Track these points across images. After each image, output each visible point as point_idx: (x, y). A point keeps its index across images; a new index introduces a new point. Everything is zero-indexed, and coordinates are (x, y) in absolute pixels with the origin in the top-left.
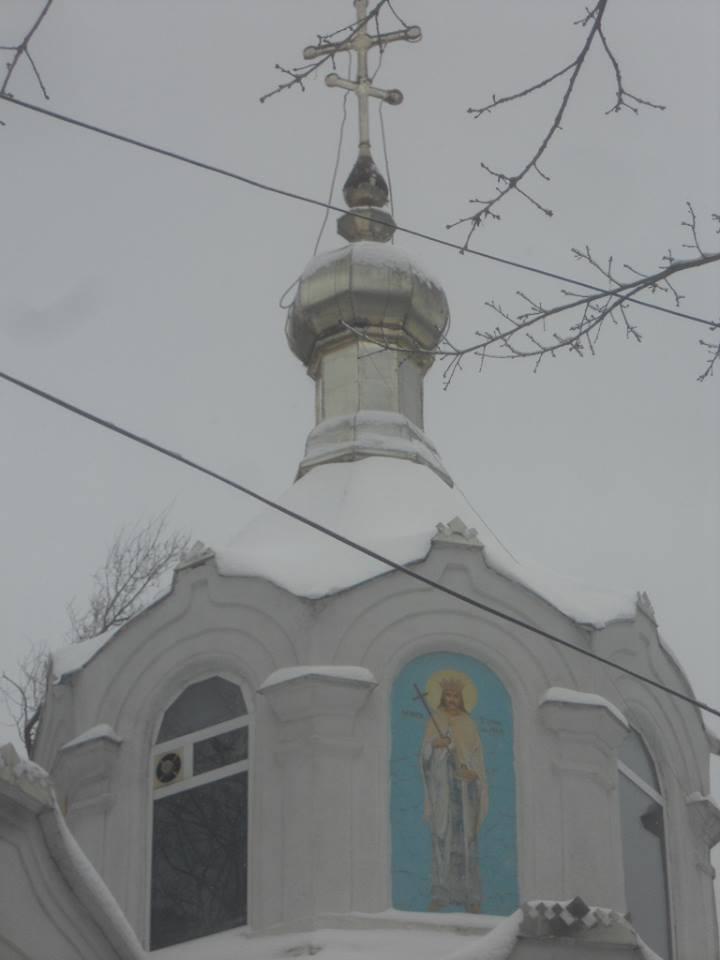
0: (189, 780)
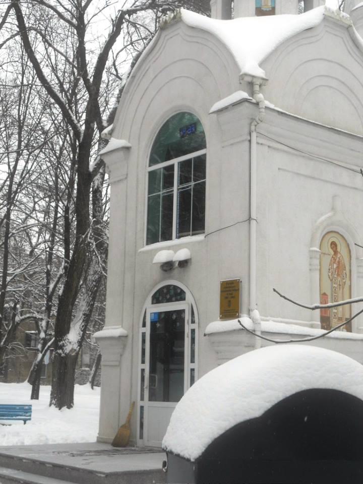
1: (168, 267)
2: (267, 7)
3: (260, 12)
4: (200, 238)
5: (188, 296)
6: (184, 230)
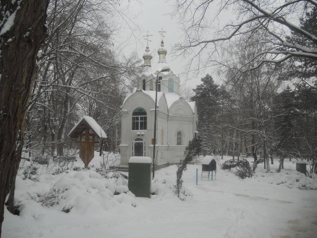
1: (139, 135)
2: (152, 89)
3: (151, 90)
5: (144, 140)
6: (141, 128)
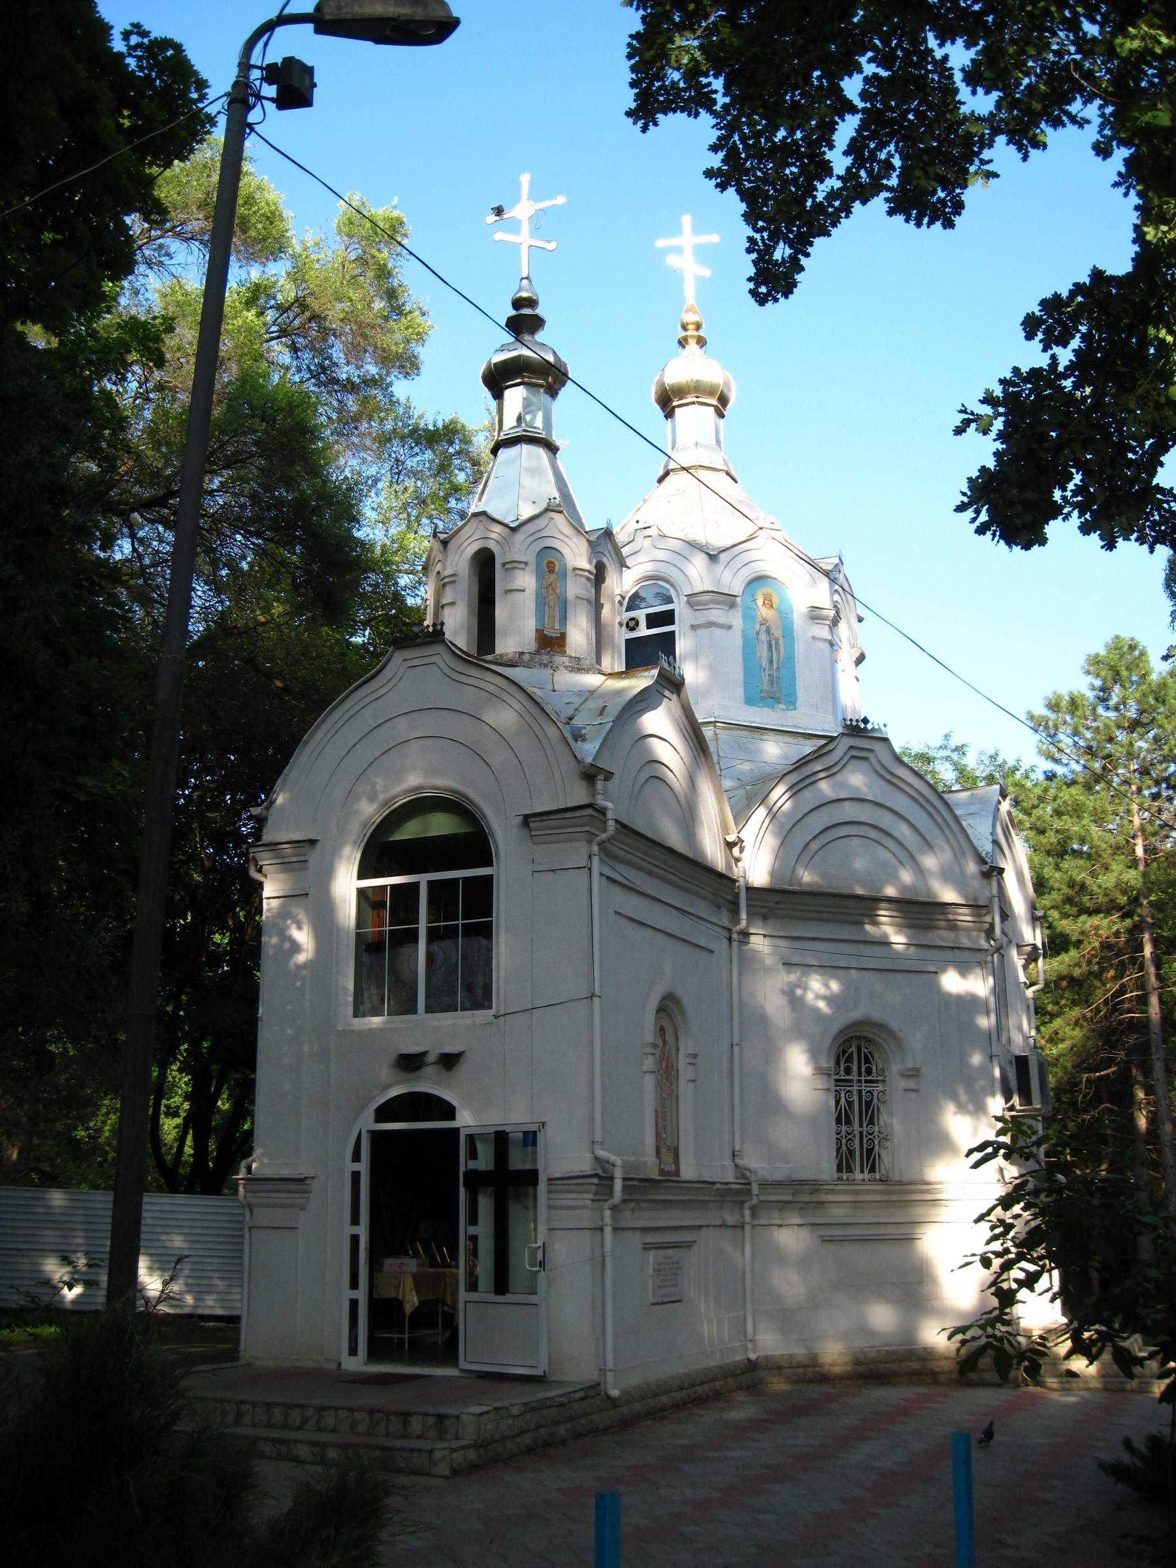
0: (643, 631)
1: (410, 1063)
4: (482, 1016)
